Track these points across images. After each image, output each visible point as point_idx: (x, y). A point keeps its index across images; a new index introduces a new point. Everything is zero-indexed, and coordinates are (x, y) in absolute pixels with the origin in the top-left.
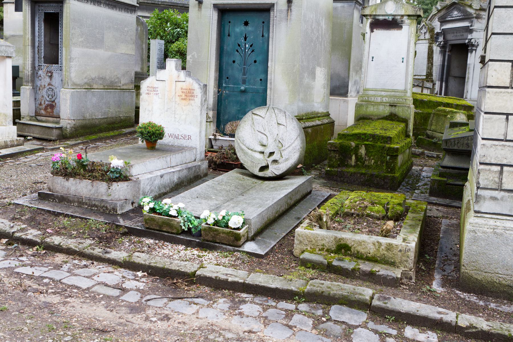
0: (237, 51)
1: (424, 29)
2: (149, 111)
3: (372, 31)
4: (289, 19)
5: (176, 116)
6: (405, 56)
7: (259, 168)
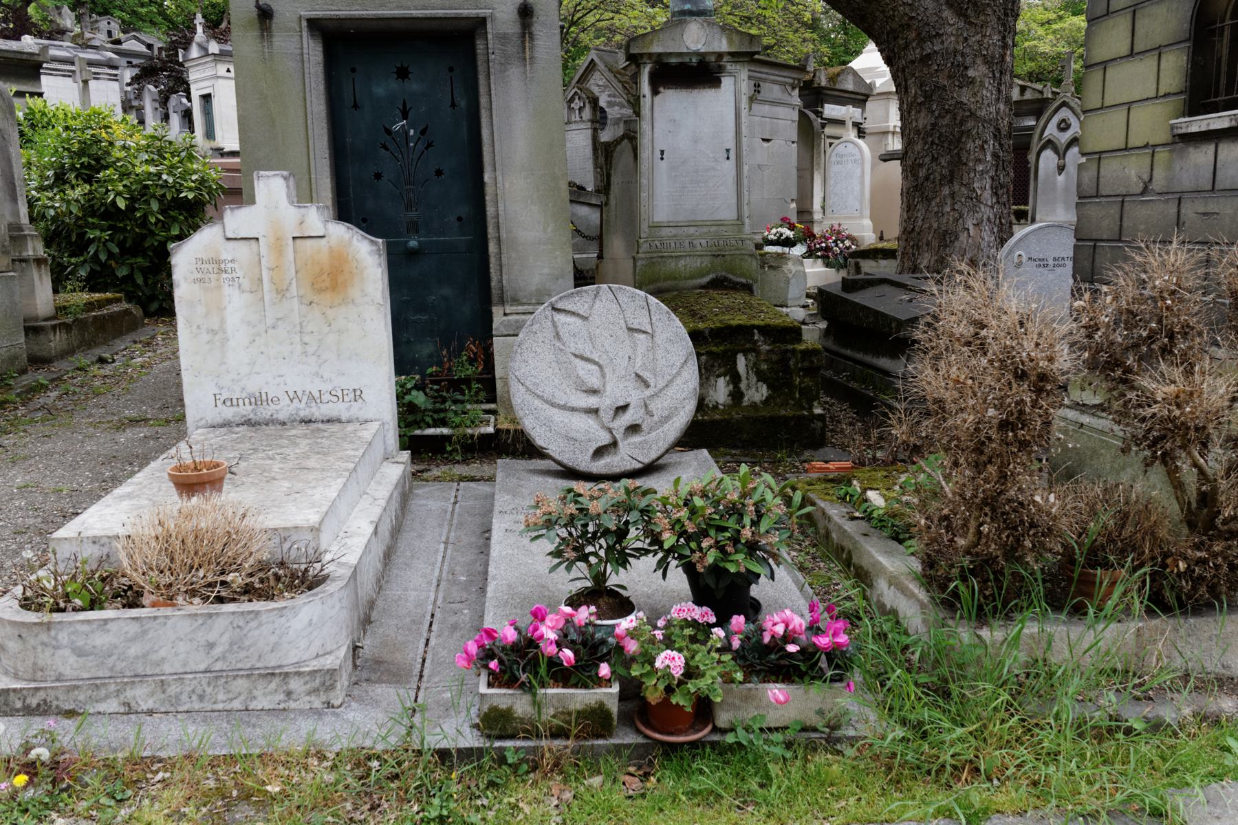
0: (385, 147)
1: (577, 101)
2: (214, 332)
3: (655, 92)
4: (528, 57)
5: (307, 339)
6: (731, 145)
7: (591, 451)
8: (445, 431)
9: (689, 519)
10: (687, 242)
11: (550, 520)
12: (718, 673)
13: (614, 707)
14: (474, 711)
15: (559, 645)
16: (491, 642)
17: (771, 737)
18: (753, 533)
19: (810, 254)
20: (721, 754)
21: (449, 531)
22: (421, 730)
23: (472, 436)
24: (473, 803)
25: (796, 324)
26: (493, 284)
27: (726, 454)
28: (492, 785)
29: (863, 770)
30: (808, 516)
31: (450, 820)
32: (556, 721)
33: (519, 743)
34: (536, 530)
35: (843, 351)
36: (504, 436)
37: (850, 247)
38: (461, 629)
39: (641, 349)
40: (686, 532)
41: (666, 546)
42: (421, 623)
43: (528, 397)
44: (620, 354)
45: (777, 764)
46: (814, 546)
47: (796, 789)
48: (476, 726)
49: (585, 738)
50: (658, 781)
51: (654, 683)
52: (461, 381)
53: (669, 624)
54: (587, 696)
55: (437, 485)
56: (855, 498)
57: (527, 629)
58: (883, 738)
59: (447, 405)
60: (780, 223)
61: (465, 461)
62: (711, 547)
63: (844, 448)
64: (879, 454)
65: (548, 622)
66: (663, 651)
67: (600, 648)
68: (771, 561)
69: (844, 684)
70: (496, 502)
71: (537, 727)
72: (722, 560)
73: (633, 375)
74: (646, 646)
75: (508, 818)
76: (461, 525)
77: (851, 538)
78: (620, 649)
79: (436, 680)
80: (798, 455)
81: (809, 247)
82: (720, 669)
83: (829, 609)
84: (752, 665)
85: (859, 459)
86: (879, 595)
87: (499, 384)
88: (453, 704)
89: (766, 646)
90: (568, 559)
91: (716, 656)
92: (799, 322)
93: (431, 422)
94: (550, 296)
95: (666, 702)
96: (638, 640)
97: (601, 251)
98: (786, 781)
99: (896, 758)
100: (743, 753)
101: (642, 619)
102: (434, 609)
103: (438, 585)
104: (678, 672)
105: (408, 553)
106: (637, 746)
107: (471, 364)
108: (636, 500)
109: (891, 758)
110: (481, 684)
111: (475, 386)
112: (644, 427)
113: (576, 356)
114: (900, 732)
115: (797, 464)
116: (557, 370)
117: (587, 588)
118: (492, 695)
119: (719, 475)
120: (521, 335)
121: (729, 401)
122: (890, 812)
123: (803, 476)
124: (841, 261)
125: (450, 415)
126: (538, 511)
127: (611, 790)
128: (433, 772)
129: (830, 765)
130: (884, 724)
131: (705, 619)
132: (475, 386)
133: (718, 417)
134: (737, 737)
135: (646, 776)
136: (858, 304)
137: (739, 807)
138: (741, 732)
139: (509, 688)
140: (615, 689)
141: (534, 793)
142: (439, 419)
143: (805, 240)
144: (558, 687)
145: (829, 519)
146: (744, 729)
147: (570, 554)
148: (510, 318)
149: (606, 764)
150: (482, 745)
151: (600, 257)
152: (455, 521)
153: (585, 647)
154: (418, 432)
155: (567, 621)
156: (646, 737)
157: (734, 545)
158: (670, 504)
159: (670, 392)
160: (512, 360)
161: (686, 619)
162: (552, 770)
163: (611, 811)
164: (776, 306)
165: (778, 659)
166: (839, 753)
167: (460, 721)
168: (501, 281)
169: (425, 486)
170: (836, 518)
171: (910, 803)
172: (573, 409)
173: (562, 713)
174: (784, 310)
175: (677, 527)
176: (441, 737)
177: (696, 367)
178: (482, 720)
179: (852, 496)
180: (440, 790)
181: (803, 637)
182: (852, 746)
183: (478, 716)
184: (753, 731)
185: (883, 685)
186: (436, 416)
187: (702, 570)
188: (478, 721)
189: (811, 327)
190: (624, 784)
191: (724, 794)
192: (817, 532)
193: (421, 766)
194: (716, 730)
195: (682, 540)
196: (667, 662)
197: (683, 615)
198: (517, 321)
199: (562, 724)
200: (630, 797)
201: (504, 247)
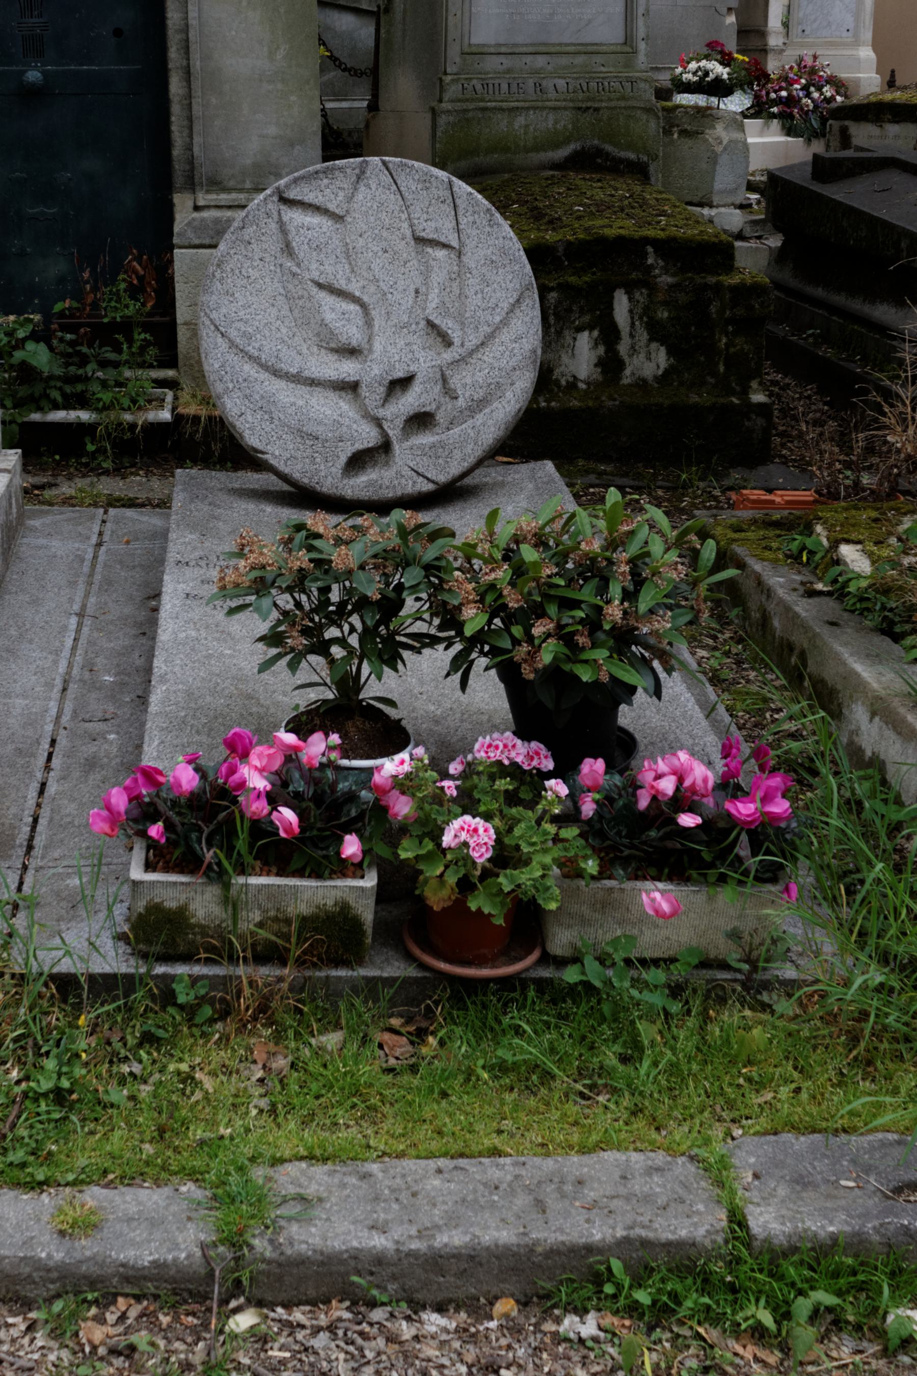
7: (343, 459)
8: (84, 416)
9: (512, 584)
10: (531, 82)
11: (262, 578)
12: (554, 860)
13: (367, 913)
14: (120, 911)
15: (273, 799)
16: (153, 791)
17: (644, 975)
18: (625, 613)
19: (758, 110)
20: (554, 1002)
21: (87, 595)
22: (26, 941)
23: (133, 426)
24: (115, 1069)
25: (724, 237)
26: (176, 152)
27: (587, 472)
28: (148, 1039)
29: (808, 1039)
30: (731, 586)
31: (74, 1096)
32: (263, 933)
33: (198, 970)
34: (238, 596)
35: (810, 290)
36: (189, 429)
37: (833, 98)
38: (102, 767)
39: (438, 277)
40: (504, 606)
41: (468, 631)
42: (33, 755)
43: (233, 359)
44: (401, 284)
45: (654, 1022)
46: (740, 641)
47: (685, 1068)
48: (121, 937)
49: (315, 965)
50: (442, 1043)
51: (438, 873)
52: (114, 326)
53: (470, 770)
54: (320, 892)
55: (69, 512)
56: (818, 557)
57: (217, 771)
58: (847, 983)
59: (89, 368)
60: (705, 51)
61: (119, 471)
62: (548, 635)
63: (803, 466)
64: (866, 479)
65: (255, 761)
66: (456, 817)
67: (345, 809)
68: (656, 664)
69: (779, 887)
70: (171, 544)
71: (231, 943)
72: (569, 659)
73: (423, 323)
74: (427, 807)
75: (174, 1098)
76: (108, 582)
77: (805, 628)
78: (380, 810)
79: (56, 854)
80: (719, 477)
81: (757, 97)
82: (557, 852)
83: (758, 754)
84: (614, 848)
85: (828, 487)
86: (852, 733)
87: (182, 334)
88: (84, 897)
89: (643, 815)
90: (292, 650)
91: (551, 828)
92: (732, 235)
93: (59, 399)
94: (279, 176)
95: (459, 907)
96: (413, 795)
97: (375, 96)
98: (669, 1052)
99: (866, 1020)
100: (594, 1001)
101: (421, 760)
102: (55, 731)
103: (64, 690)
104: (481, 856)
105: (13, 632)
106: (407, 981)
107: (133, 297)
108: (417, 547)
109: (858, 1020)
110: (133, 864)
111: (140, 336)
112: (440, 417)
113: (320, 286)
114: (877, 976)
115: (717, 493)
116: (285, 312)
117: (325, 701)
118: (153, 883)
119: (571, 506)
120: (222, 247)
121: (597, 375)
122: (852, 1113)
123: (724, 515)
124: (815, 124)
125: (95, 387)
126: (242, 563)
127: (357, 1057)
128: (47, 1013)
129: (747, 1029)
130: (850, 961)
131: (535, 763)
132: (140, 336)
133: (575, 403)
134: (583, 973)
135: (420, 1035)
136: (840, 203)
137: (582, 1095)
138: (591, 964)
139: (182, 872)
140: (370, 881)
141: (221, 1056)
142: (74, 395)
143: (751, 85)
144: (268, 875)
145: (768, 592)
146: (598, 959)
147: (297, 641)
148: (205, 214)
149: (349, 1011)
150: (132, 971)
151: (373, 107)
152: (98, 577)
153: (318, 806)
154: (36, 417)
155: (288, 759)
156: (422, 966)
157: (591, 634)
158: (480, 557)
159: (488, 355)
160: (205, 291)
161: (499, 763)
162: (255, 1018)
163: (357, 1093)
164: (690, 203)
165: (662, 839)
166: (766, 1007)
167: (96, 927)
168: (189, 147)
169: (47, 512)
170: (781, 592)
171: (888, 1099)
172: (313, 383)
173: (276, 919)
174: (706, 211)
175: (489, 599)
176: (61, 953)
177: (537, 312)
178: (133, 928)
179: (811, 553)
180: (58, 1046)
181: (709, 802)
182: (790, 996)
183: (128, 920)
184: (614, 964)
185: (850, 892)
186: (68, 389)
187: (532, 676)
188: (126, 928)
189: (753, 244)
190: (381, 1046)
191: (556, 1070)
192: (746, 617)
193: (26, 1002)
194: (546, 959)
195: (497, 621)
196: (464, 836)
197: (494, 755)
198: (217, 221)
199: (273, 938)
200: (391, 1070)
201: (196, 85)
